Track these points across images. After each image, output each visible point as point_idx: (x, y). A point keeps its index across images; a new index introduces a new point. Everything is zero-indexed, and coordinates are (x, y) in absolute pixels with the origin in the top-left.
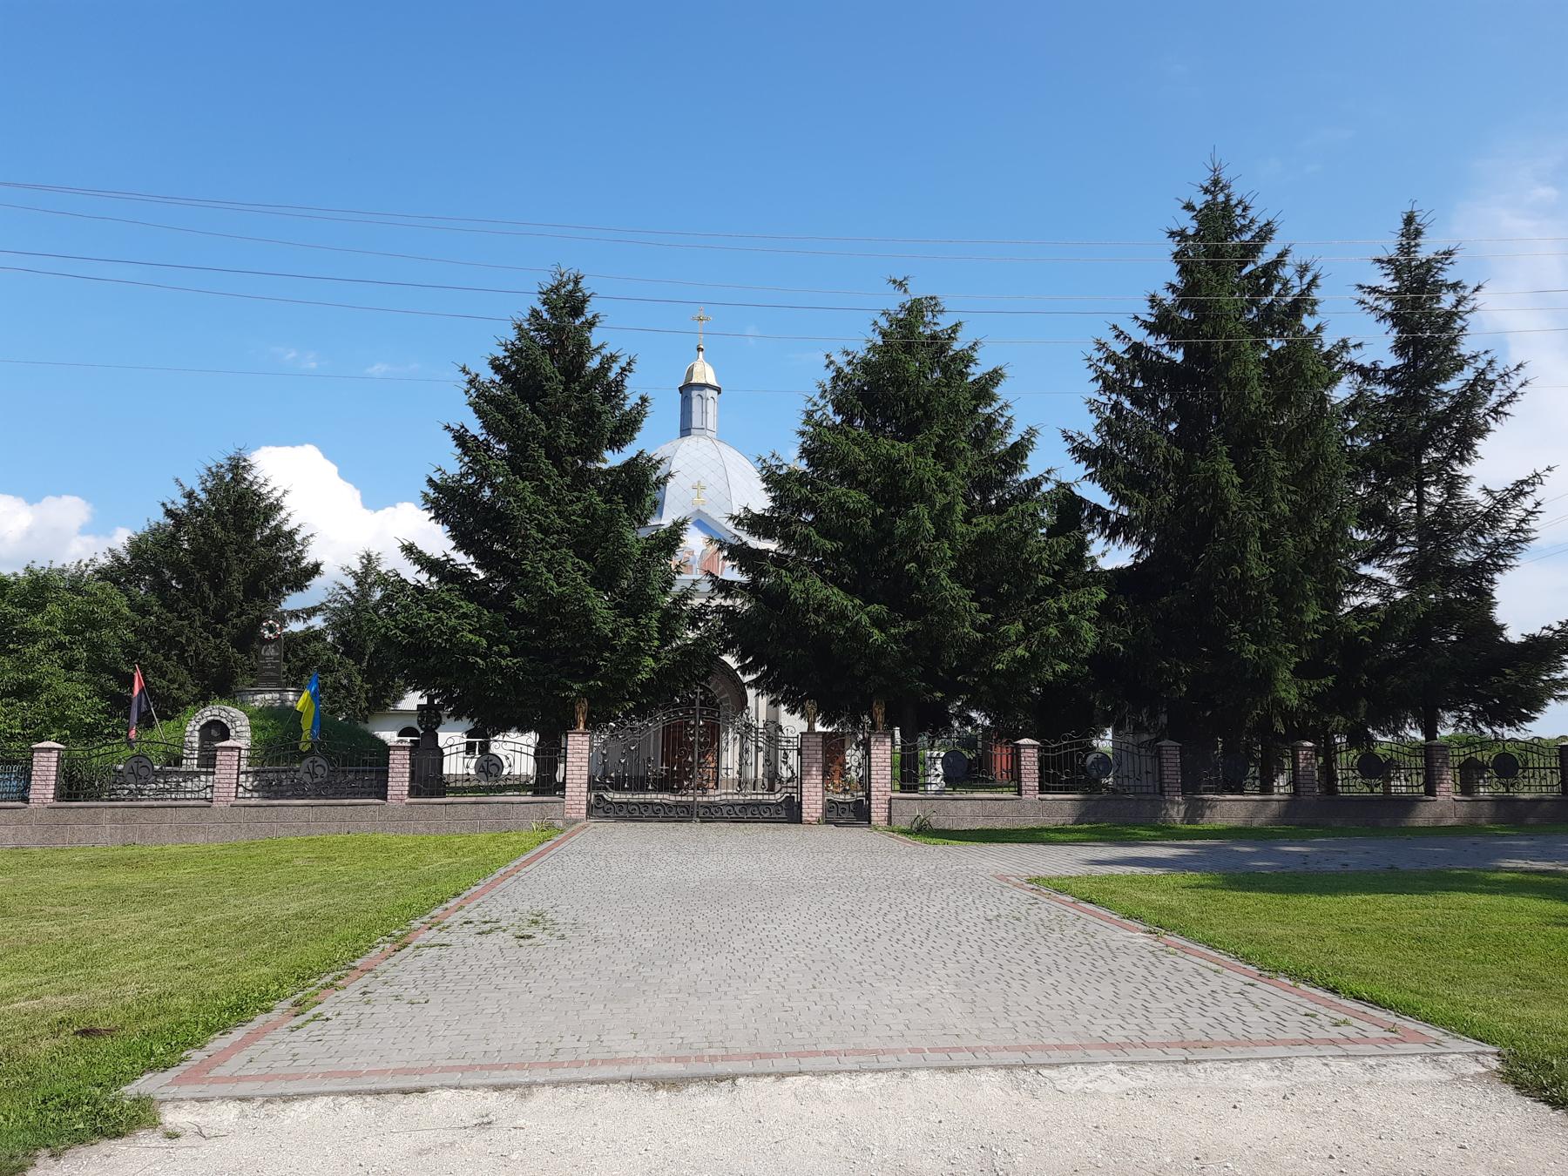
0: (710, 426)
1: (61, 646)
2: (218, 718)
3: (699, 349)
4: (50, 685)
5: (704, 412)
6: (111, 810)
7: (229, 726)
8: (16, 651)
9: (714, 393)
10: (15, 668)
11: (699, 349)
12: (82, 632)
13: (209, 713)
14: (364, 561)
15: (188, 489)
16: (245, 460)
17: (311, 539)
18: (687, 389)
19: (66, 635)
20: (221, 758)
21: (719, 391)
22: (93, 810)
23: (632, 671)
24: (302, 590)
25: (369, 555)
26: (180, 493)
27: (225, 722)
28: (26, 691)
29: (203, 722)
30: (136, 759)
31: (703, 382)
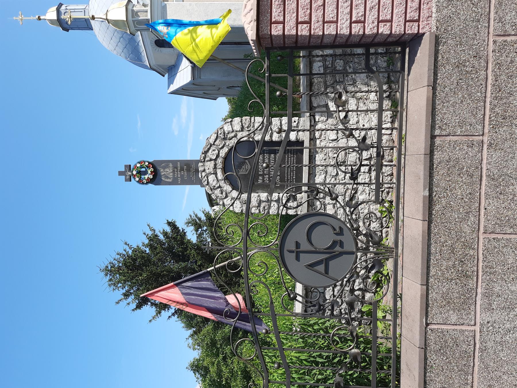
0: (84, 7)
1: (224, 359)
2: (220, 161)
3: (39, 19)
4: (244, 363)
5: (74, 11)
6: (433, 311)
7: (232, 143)
8: (226, 379)
9: (63, 8)
10: (235, 380)
11: (39, 19)
12: (218, 349)
13: (211, 178)
14: (190, 225)
15: (123, 297)
16: (107, 267)
17: (151, 226)
18: (60, 22)
19: (219, 356)
20: (290, 24)
21: (60, 5)
22: (432, 357)
23: (292, 384)
24: (185, 233)
25: (187, 223)
26: (124, 301)
27: (226, 150)
28: (247, 376)
29: (227, 188)
30: (290, 258)
31: (56, 12)
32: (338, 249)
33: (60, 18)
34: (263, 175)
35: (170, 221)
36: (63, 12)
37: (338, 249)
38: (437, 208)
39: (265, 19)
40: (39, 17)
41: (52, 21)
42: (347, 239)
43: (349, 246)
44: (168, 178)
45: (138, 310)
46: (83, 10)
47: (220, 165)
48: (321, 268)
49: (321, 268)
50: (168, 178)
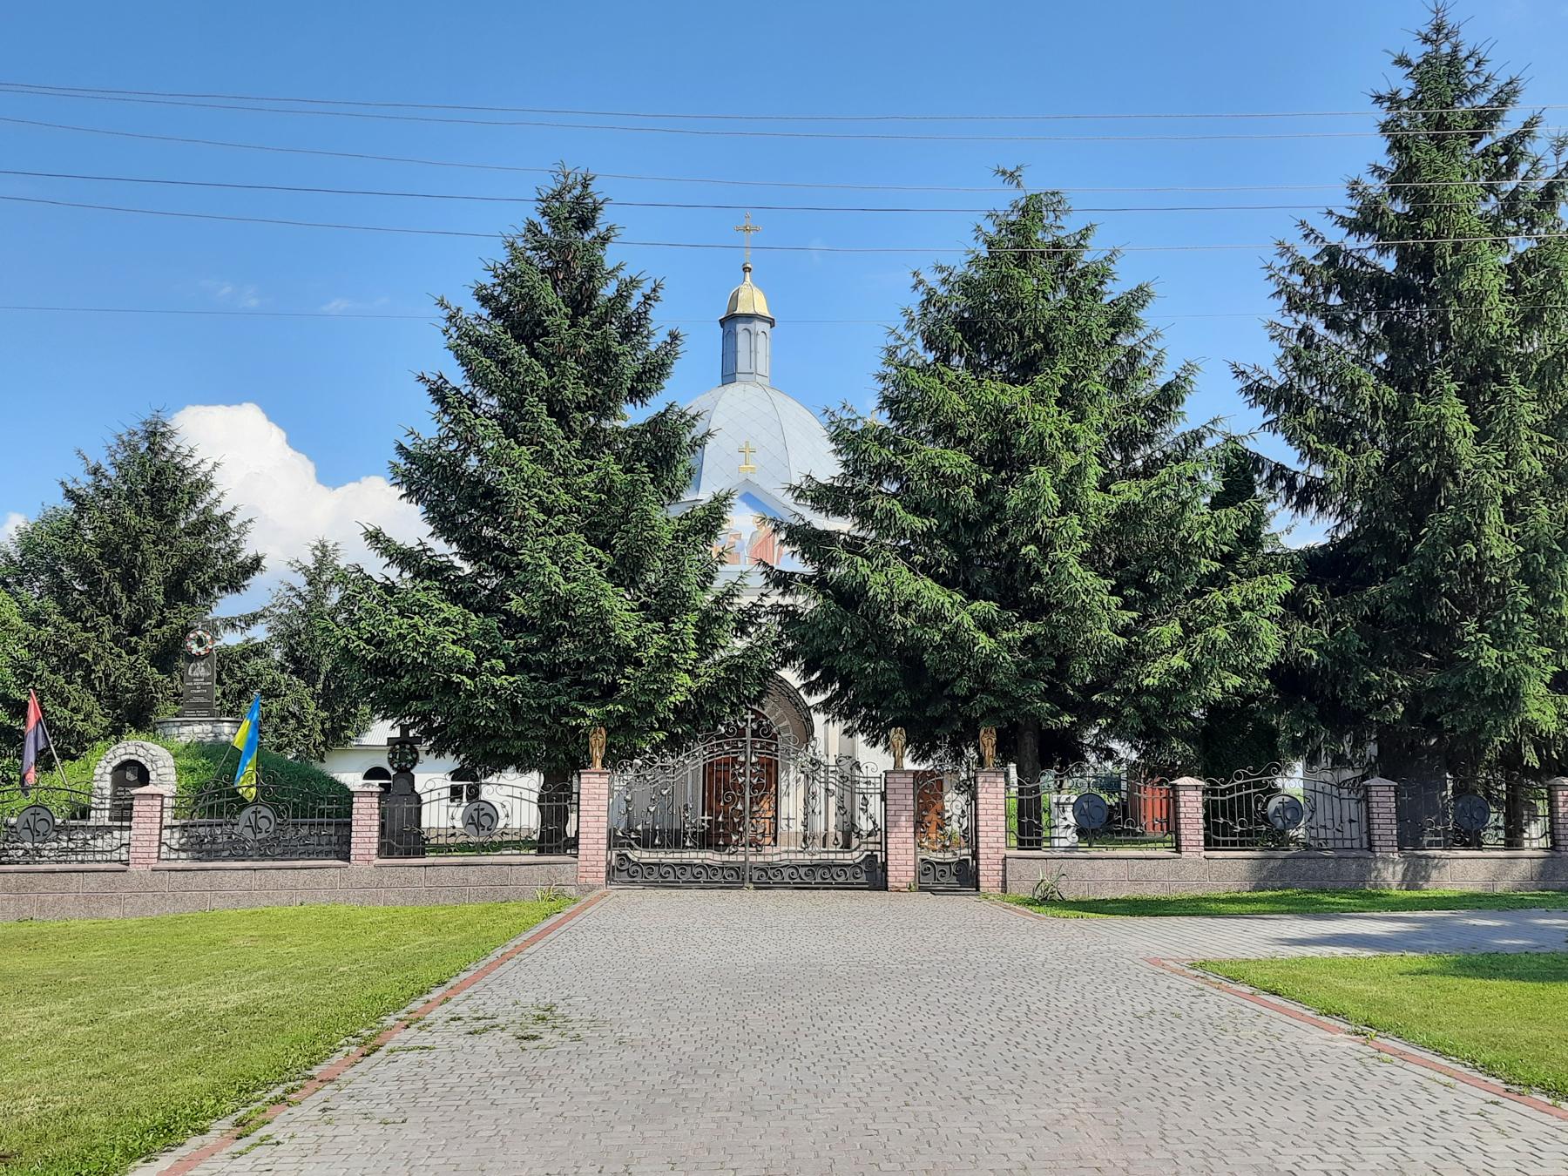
0: (761, 370)
3: (746, 269)
7: (148, 767)
11: (746, 269)
13: (123, 751)
14: (317, 552)
15: (93, 463)
18: (730, 320)
24: (238, 591)
25: (323, 546)
26: (84, 468)
32: (36, 833)
33: (739, 320)
34: (124, 791)
35: (264, 562)
36: (750, 326)
37: (36, 833)
38: (51, 875)
39: (141, 797)
40: (750, 269)
41: (735, 299)
42: (41, 838)
43: (37, 839)
44: (193, 670)
45: (61, 491)
46: (753, 370)
47: (132, 757)
48: (26, 826)
49: (26, 826)
50: (193, 670)
